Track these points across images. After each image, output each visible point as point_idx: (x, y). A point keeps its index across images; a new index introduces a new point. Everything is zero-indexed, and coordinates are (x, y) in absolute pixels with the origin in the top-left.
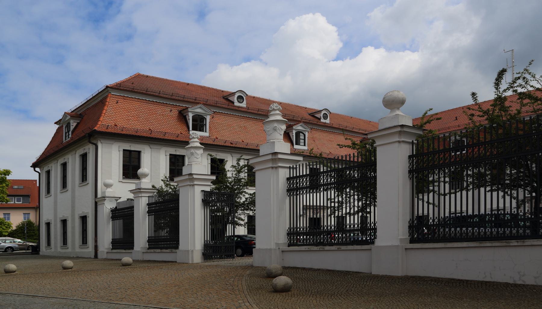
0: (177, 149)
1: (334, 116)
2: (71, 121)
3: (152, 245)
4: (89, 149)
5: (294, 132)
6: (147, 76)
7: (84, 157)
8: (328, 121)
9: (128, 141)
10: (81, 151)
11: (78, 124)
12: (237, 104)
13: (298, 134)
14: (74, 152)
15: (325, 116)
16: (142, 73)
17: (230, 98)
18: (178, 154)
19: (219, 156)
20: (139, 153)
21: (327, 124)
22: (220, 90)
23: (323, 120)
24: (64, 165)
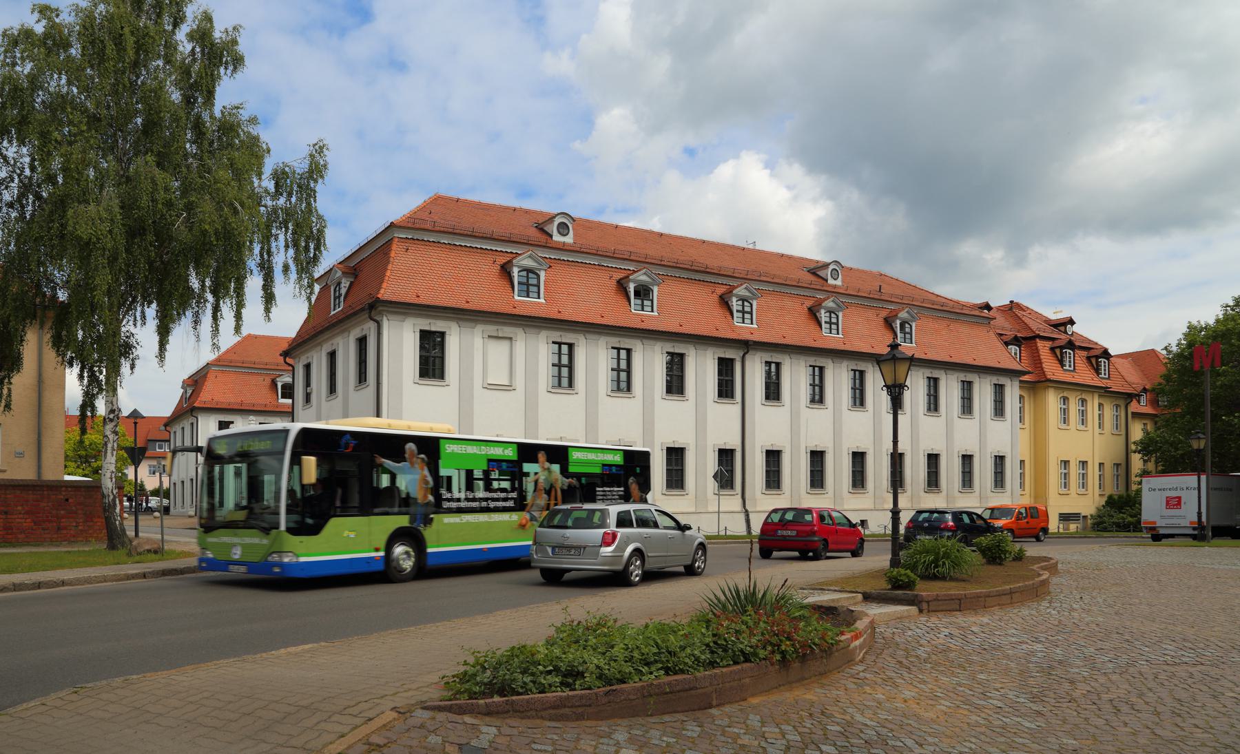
0: (432, 321)
1: (585, 226)
2: (343, 281)
3: (344, 501)
4: (370, 328)
5: (898, 322)
6: (458, 200)
7: (362, 342)
8: (569, 239)
9: (722, 346)
10: (356, 333)
11: (352, 284)
12: (557, 238)
13: (902, 326)
14: (346, 334)
15: (563, 229)
16: (443, 193)
17: (821, 273)
18: (433, 329)
19: (436, 325)
20: (442, 334)
21: (569, 245)
22: (451, 199)
23: (831, 281)
24: (332, 356)
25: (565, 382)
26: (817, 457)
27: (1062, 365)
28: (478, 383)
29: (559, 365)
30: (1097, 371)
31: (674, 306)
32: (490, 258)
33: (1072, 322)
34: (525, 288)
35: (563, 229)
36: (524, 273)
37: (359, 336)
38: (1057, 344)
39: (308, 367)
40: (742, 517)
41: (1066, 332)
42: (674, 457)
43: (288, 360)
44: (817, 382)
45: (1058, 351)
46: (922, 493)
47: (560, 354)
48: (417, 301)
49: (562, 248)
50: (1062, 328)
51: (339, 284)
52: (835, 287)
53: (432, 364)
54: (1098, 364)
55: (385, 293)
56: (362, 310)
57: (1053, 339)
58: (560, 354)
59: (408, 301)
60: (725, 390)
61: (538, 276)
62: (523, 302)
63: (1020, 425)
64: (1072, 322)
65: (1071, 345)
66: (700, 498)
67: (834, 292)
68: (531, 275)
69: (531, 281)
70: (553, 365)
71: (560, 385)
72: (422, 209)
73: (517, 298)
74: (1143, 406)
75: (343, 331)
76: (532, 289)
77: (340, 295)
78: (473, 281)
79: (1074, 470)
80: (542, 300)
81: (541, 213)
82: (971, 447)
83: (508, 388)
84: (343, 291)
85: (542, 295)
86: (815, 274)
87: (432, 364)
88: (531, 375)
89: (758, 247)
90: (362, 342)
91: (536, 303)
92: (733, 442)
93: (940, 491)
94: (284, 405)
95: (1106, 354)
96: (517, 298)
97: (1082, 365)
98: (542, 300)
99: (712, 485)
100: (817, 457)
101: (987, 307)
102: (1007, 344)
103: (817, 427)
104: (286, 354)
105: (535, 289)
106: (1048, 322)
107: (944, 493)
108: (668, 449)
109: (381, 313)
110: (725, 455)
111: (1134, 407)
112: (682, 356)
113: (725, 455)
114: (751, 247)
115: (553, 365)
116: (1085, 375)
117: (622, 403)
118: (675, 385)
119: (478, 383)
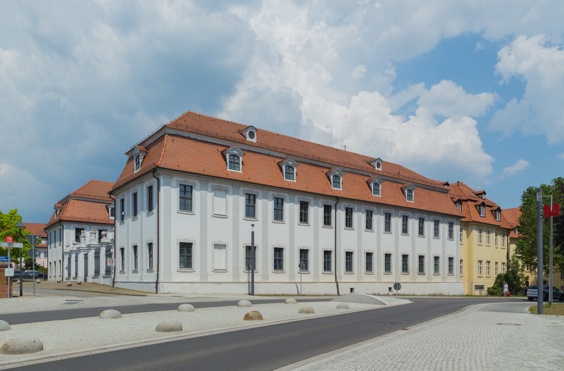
1: (264, 134)
7: (150, 188)
15: (252, 135)
21: (254, 143)
23: (377, 169)
24: (135, 195)
26: (304, 253)
27: (480, 214)
28: (209, 214)
30: (495, 218)
31: (314, 180)
32: (216, 147)
33: (484, 193)
35: (252, 135)
36: (232, 157)
37: (149, 185)
38: (478, 203)
39: (123, 201)
40: (336, 284)
41: (482, 198)
42: (278, 253)
43: (112, 196)
45: (478, 207)
46: (417, 275)
48: (178, 169)
49: (251, 144)
50: (480, 196)
51: (138, 156)
52: (378, 171)
53: (186, 204)
54: (480, 210)
55: (162, 163)
56: (150, 171)
57: (476, 201)
59: (173, 168)
60: (327, 221)
62: (232, 172)
63: (460, 243)
64: (484, 193)
65: (483, 204)
66: (292, 276)
67: (378, 174)
68: (236, 158)
72: (181, 118)
73: (228, 170)
74: (515, 234)
75: (140, 183)
77: (139, 163)
78: (207, 159)
79: (484, 265)
80: (241, 172)
81: (241, 125)
83: (224, 217)
84: (141, 161)
86: (369, 164)
87: (186, 204)
88: (236, 210)
89: (347, 150)
90: (150, 188)
91: (239, 172)
92: (331, 247)
93: (408, 274)
94: (112, 220)
95: (499, 210)
96: (228, 170)
97: (489, 214)
98: (241, 172)
99: (297, 269)
100: (304, 253)
101: (447, 184)
102: (455, 203)
104: (110, 193)
106: (474, 192)
107: (411, 274)
108: (180, 243)
109: (159, 174)
110: (327, 253)
111: (512, 234)
113: (327, 253)
114: (343, 149)
116: (489, 219)
117: (278, 226)
118: (304, 218)
119: (209, 214)
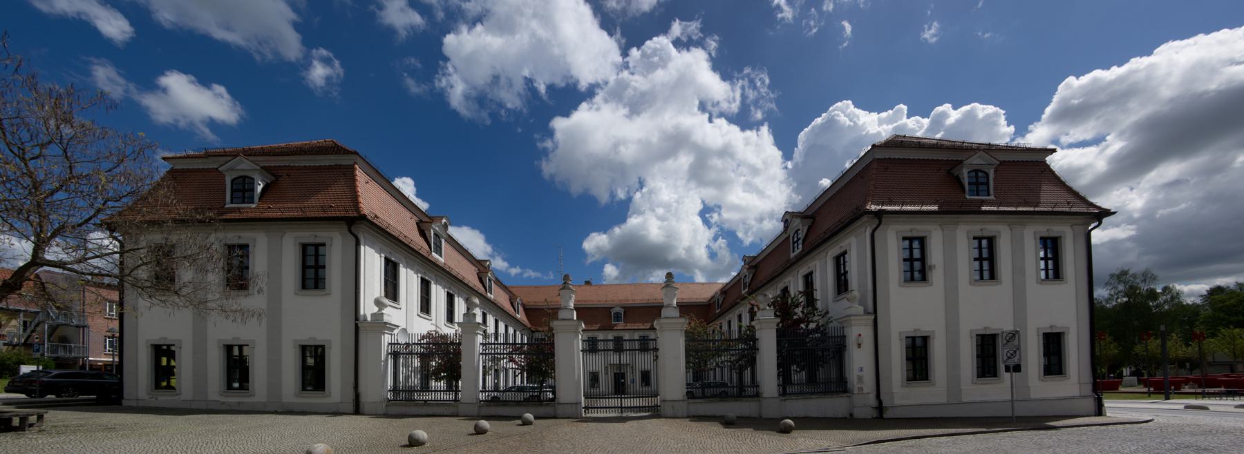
5: (965, 172)
25: (986, 275)
29: (980, 259)
34: (974, 187)
44: (985, 254)
47: (911, 249)
58: (911, 249)
61: (987, 175)
68: (980, 174)
69: (981, 180)
70: (905, 260)
71: (982, 278)
76: (981, 187)
80: (992, 197)
82: (1001, 323)
85: (992, 191)
103: (987, 308)
105: (985, 187)
112: (244, 247)
115: (905, 260)
